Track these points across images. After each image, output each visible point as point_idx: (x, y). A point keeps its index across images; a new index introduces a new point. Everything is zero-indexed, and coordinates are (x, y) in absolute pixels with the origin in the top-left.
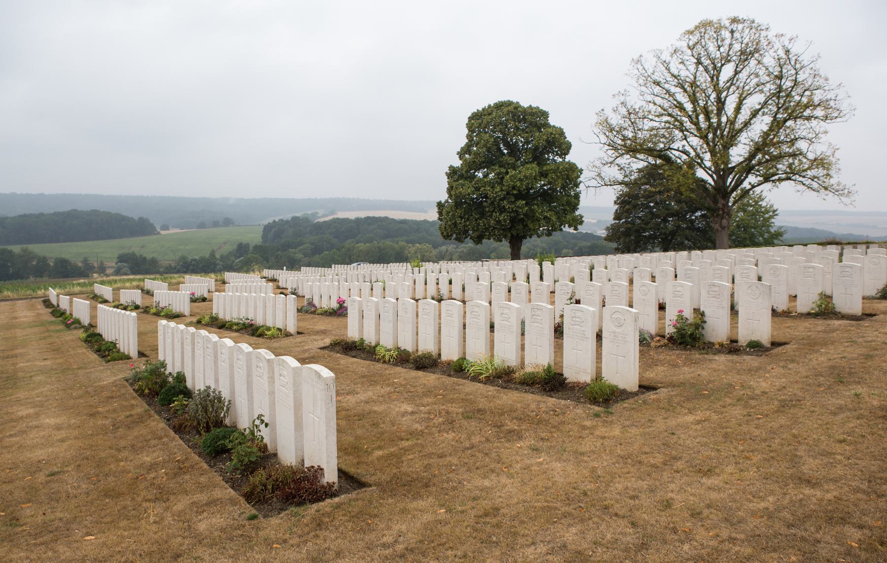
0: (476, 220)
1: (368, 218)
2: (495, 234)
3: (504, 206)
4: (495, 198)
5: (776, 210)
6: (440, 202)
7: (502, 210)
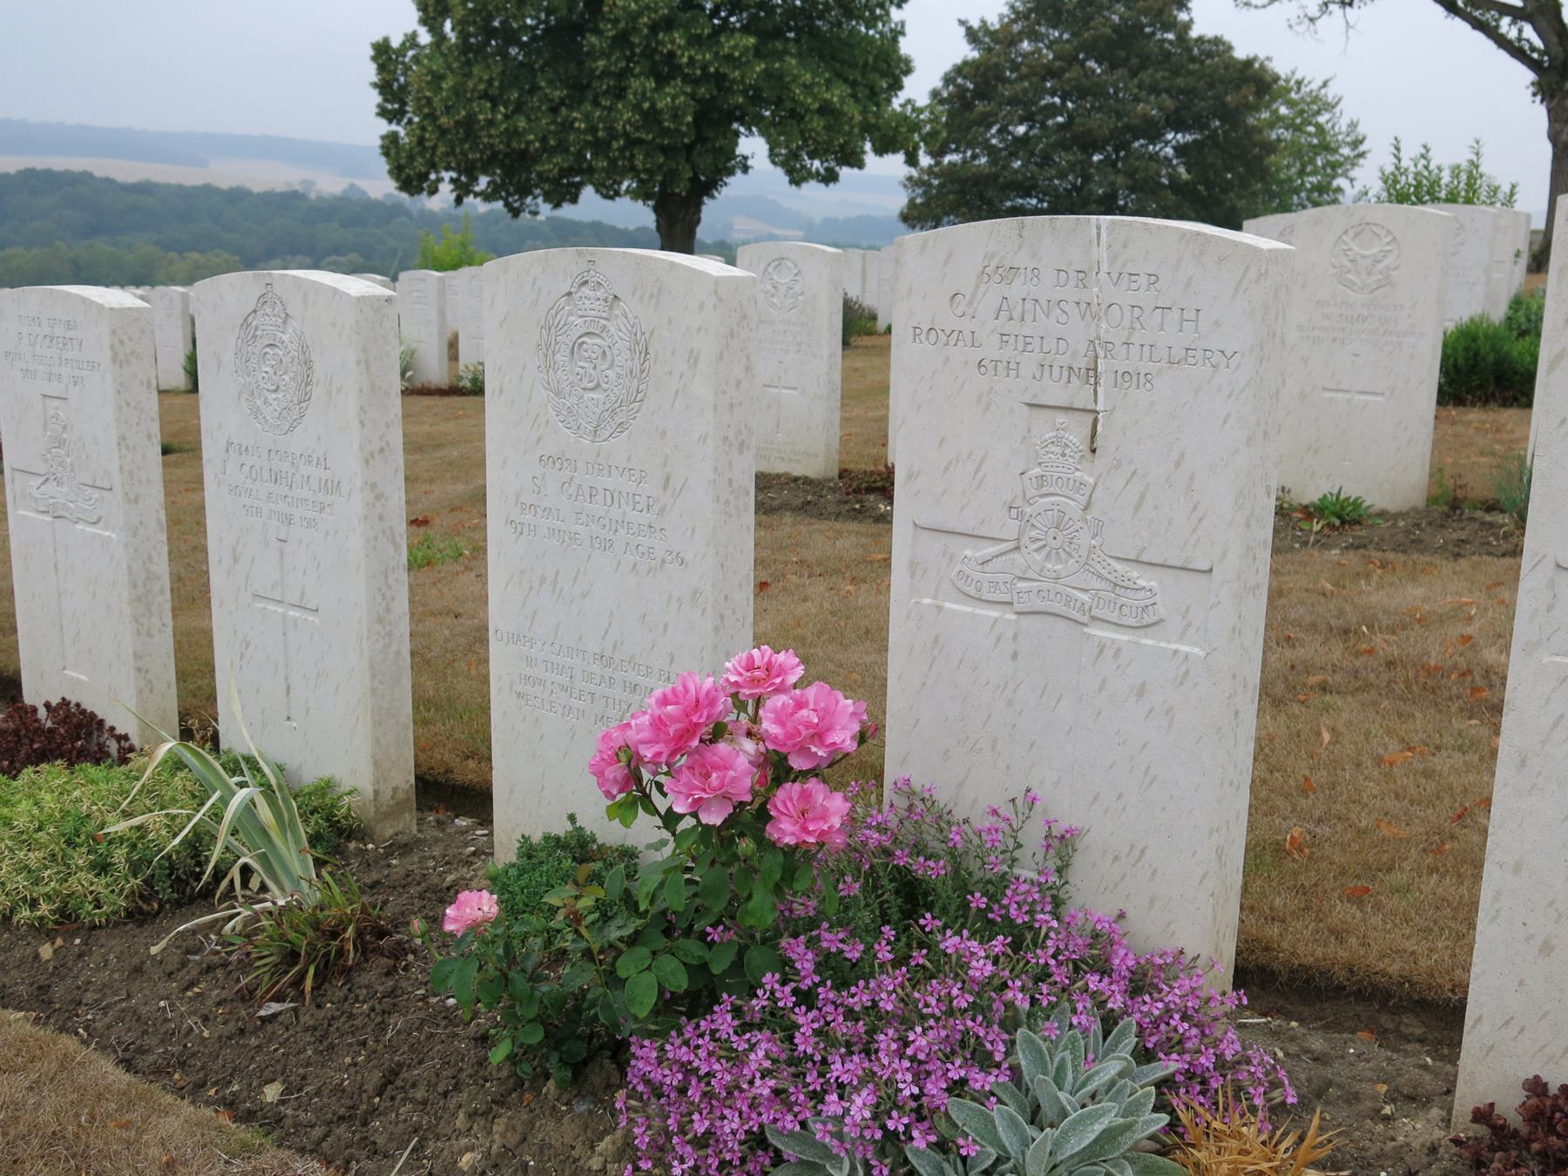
0: (554, 110)
1: (29, 174)
2: (633, 169)
3: (672, 54)
4: (635, 17)
5: (1361, 142)
6: (386, 41)
7: (664, 70)
